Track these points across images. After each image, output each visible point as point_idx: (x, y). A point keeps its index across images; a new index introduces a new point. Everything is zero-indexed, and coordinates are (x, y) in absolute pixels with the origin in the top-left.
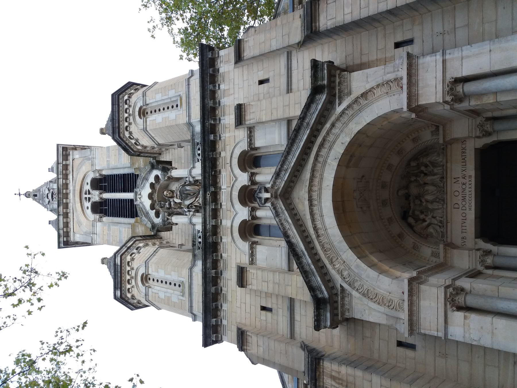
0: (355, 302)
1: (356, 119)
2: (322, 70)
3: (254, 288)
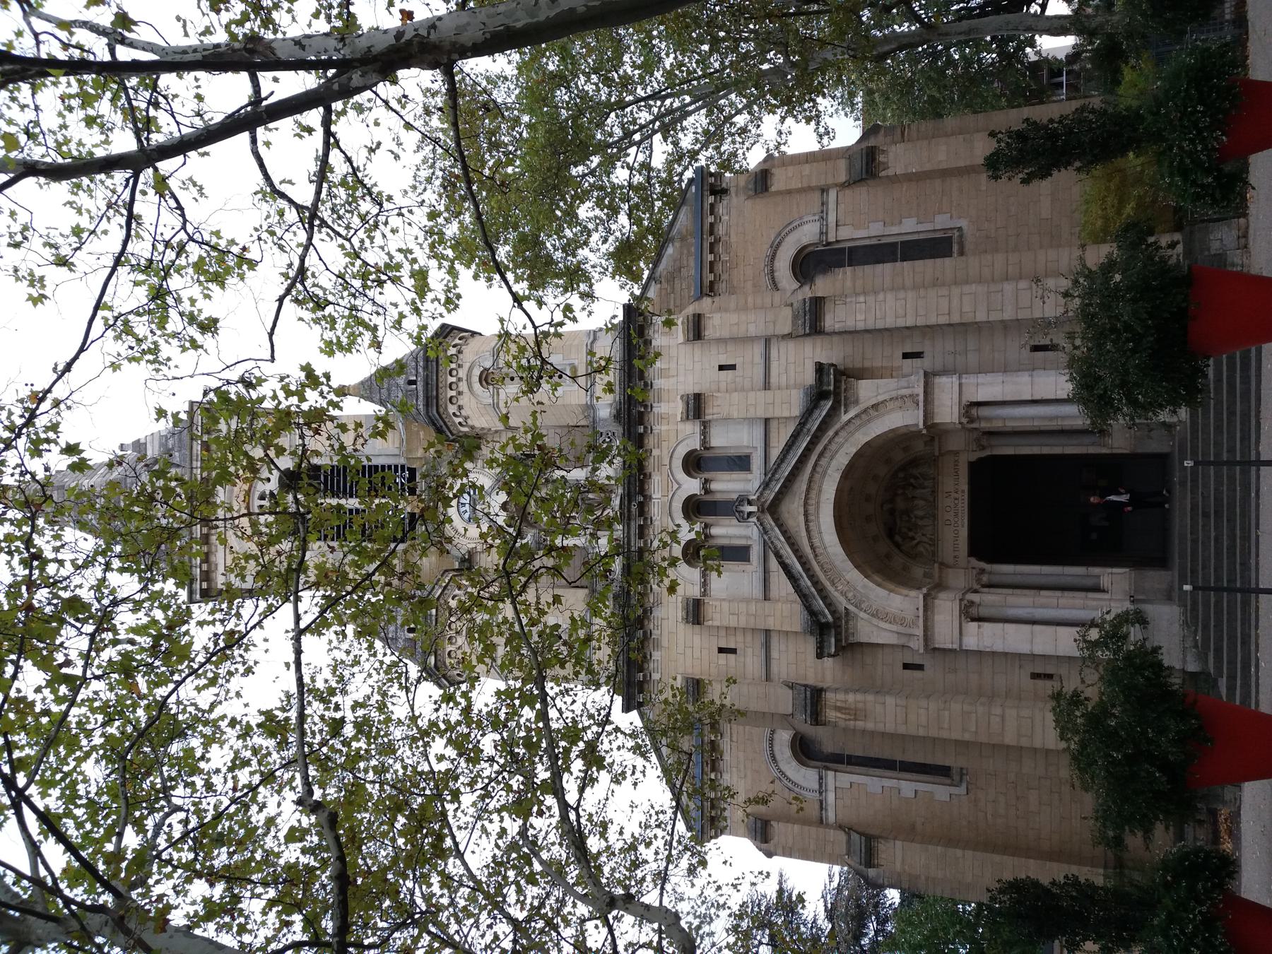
0: (860, 624)
1: (863, 430)
2: (828, 375)
3: (717, 623)
